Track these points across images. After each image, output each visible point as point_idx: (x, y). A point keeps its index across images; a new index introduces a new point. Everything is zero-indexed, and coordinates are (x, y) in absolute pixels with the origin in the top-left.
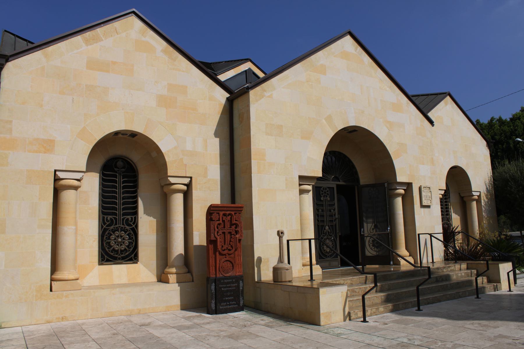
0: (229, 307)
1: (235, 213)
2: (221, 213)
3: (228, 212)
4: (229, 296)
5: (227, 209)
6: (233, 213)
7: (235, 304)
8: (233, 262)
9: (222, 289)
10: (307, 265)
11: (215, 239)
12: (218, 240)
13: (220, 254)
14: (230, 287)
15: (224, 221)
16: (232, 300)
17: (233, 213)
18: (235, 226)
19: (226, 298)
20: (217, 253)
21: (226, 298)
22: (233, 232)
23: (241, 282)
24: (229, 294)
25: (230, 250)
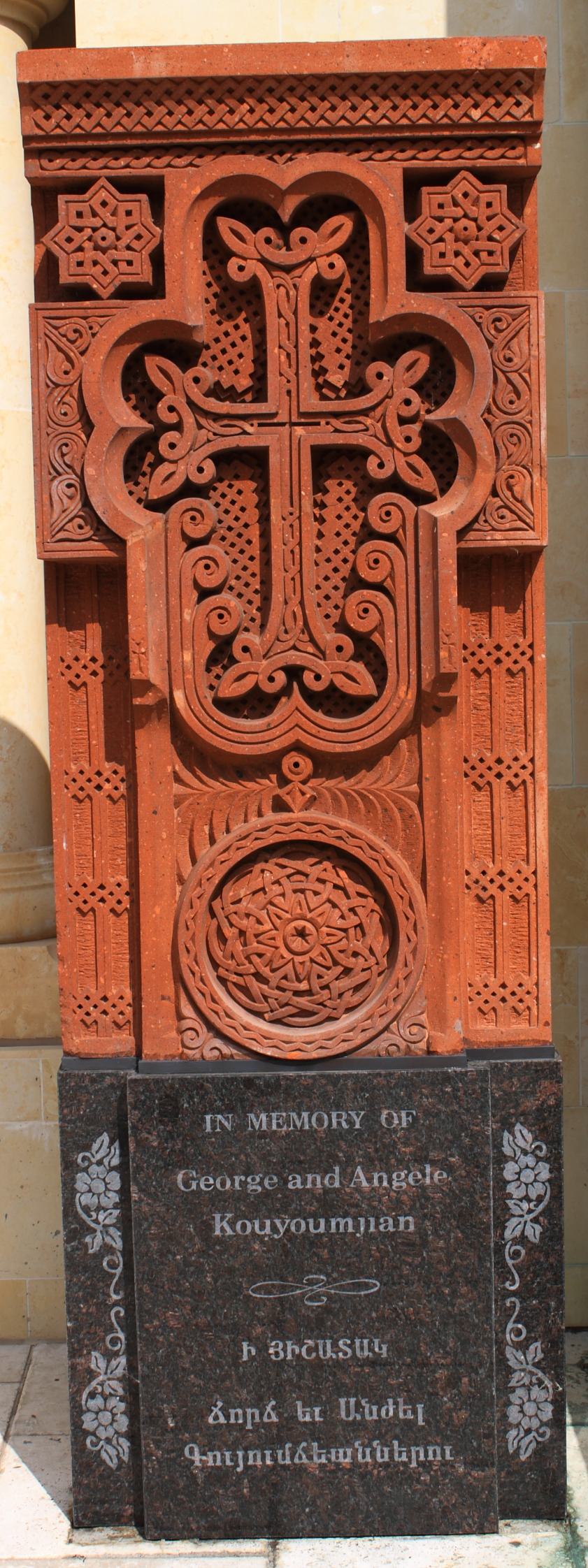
0: (315, 1458)
1: (414, 183)
2: (187, 183)
3: (286, 172)
4: (318, 1325)
5: (283, 115)
6: (382, 177)
7: (408, 1433)
8: (396, 865)
9: (221, 1226)
10: (61, 1341)
11: (97, 550)
12: (139, 568)
13: (196, 754)
14: (328, 1204)
15: (238, 299)
16: (369, 1380)
17: (382, 177)
18: (418, 361)
19: (283, 1350)
20: (154, 745)
21: (283, 1350)
22: (396, 457)
23: (521, 1137)
24: (315, 1290)
25: (333, 701)
